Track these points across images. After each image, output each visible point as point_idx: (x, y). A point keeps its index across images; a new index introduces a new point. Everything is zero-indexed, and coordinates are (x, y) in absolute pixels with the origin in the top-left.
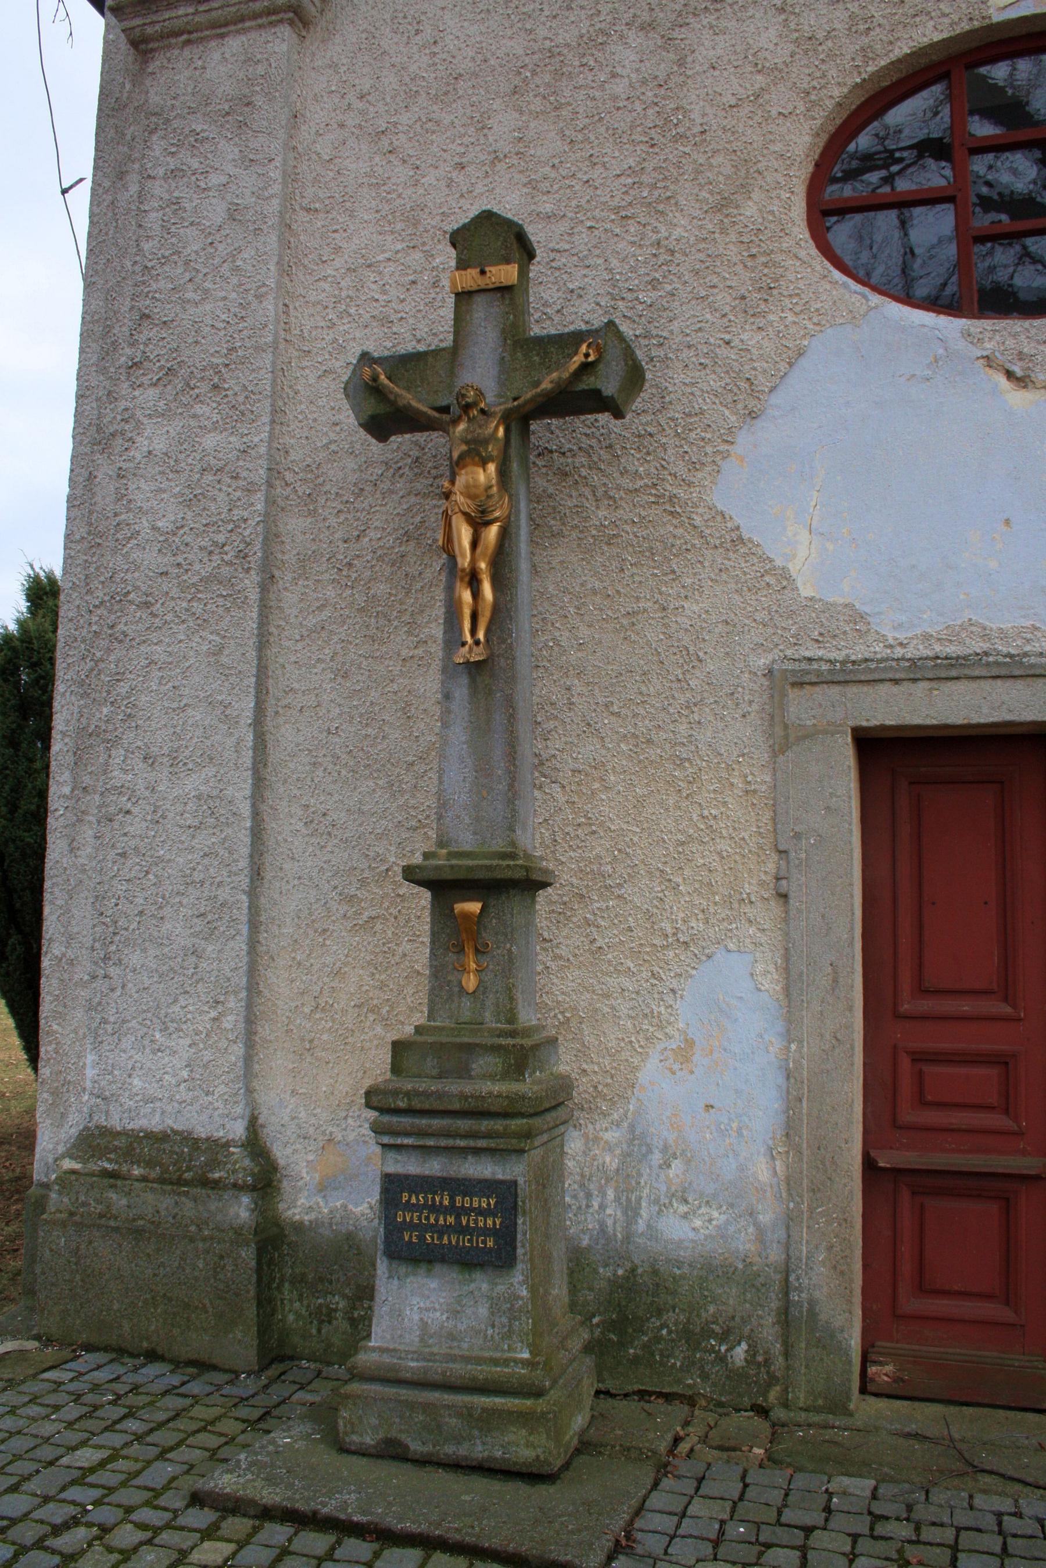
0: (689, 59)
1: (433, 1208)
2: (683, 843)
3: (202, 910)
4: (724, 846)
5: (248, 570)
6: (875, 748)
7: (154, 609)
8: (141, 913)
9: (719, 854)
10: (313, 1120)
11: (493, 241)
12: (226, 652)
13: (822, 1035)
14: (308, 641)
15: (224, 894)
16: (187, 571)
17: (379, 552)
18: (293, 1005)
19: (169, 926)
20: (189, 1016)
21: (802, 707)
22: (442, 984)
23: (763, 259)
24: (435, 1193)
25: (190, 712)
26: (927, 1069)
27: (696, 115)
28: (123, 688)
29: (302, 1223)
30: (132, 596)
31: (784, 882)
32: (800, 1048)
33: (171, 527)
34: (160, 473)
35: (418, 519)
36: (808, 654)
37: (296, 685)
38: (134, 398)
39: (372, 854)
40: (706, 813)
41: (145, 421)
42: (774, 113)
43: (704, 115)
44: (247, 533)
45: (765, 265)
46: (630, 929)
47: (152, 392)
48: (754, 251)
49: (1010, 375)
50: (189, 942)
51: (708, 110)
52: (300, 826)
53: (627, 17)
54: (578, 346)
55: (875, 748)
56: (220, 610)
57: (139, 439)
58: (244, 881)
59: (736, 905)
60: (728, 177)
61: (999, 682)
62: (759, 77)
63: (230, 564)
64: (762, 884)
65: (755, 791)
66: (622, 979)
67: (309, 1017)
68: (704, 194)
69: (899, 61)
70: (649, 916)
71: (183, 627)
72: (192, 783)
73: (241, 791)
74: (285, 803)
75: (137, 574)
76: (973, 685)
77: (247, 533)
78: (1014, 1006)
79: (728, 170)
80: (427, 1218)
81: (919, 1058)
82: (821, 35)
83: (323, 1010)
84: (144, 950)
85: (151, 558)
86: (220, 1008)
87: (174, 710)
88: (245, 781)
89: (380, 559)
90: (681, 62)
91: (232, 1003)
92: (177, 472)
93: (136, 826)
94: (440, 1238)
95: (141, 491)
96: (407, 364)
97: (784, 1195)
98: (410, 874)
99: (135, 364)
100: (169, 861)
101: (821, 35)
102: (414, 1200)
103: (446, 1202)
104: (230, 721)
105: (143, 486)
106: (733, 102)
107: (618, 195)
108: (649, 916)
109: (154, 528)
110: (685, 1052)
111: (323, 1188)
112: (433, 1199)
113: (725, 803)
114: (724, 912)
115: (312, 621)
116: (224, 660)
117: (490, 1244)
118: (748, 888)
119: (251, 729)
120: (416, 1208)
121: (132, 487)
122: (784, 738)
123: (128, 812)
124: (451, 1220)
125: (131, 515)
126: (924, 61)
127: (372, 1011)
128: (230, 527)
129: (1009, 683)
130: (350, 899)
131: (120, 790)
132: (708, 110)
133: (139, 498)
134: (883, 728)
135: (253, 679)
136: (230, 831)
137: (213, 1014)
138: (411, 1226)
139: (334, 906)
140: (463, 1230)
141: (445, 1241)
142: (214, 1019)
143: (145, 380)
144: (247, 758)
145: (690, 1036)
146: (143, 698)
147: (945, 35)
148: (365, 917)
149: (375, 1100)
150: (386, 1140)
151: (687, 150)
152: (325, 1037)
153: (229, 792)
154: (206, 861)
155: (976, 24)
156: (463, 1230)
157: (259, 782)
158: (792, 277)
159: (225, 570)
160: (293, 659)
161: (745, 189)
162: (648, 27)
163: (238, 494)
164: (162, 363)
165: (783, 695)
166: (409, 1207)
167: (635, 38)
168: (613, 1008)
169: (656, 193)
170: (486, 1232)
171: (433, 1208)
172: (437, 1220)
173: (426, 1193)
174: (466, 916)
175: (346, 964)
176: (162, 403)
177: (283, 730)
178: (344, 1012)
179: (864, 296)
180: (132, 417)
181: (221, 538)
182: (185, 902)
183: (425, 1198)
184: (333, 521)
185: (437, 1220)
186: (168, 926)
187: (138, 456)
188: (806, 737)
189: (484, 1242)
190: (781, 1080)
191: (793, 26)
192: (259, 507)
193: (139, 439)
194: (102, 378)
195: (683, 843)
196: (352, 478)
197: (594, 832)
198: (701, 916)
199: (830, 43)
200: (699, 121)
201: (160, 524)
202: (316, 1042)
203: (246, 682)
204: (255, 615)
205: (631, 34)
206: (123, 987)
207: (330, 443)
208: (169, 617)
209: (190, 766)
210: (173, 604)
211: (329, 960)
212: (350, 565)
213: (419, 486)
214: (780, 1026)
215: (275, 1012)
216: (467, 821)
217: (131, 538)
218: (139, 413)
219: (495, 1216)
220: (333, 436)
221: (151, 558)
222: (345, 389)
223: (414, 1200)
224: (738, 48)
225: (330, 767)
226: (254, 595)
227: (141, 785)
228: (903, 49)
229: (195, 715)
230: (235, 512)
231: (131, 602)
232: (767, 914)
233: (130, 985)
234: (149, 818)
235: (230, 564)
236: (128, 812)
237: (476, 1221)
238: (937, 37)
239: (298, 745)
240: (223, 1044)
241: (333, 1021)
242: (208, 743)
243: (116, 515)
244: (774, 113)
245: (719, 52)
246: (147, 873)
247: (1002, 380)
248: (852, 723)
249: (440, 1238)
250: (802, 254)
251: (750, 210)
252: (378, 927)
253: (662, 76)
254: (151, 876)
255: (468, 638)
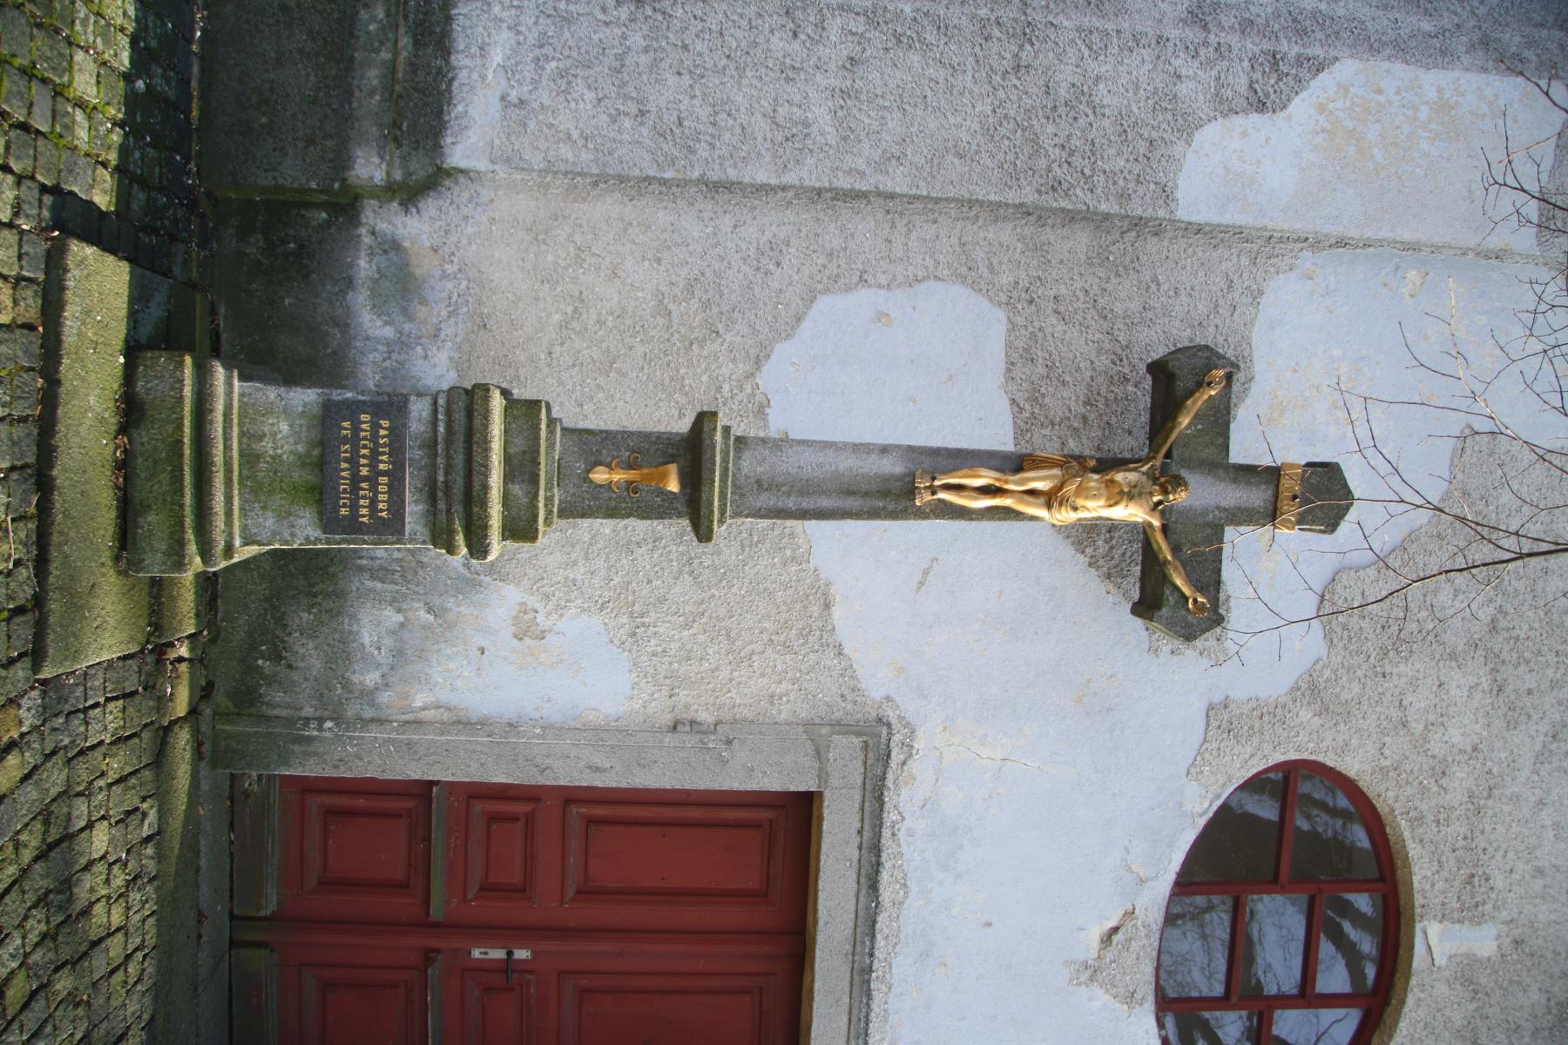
0: (1453, 664)
1: (375, 454)
2: (728, 635)
3: (686, 123)
4: (724, 673)
5: (1039, 192)
6: (801, 811)
7: (1012, 77)
8: (685, 47)
9: (717, 669)
10: (464, 241)
11: (1322, 494)
12: (956, 161)
13: (548, 756)
14: (959, 250)
15: (703, 151)
16: (1048, 118)
17: (1040, 335)
18: (584, 222)
19: (670, 82)
20: (573, 105)
21: (845, 756)
22: (595, 445)
23: (1257, 725)
24: (390, 456)
25: (898, 115)
26: (521, 824)
27: (1402, 667)
28: (930, 36)
29: (358, 224)
30: (1028, 47)
31: (688, 728)
32: (537, 736)
33: (1097, 100)
34: (1156, 89)
35: (1068, 379)
36: (894, 754)
37: (914, 235)
38: (1241, 60)
39: (736, 315)
40: (755, 658)
41: (1214, 73)
42: (1387, 740)
43: (1399, 676)
44: (1078, 191)
45: (1251, 728)
46: (650, 582)
47: (1244, 81)
48: (1266, 718)
49: (1116, 930)
50: (652, 107)
51: (1404, 680)
52: (769, 235)
53: (1508, 608)
54: (1200, 589)
55: (801, 811)
56: (1001, 156)
57: (1196, 63)
58: (715, 175)
59: (668, 681)
60: (1338, 696)
61: (852, 916)
62: (1421, 727)
63: (1049, 170)
64: (687, 706)
65: (772, 703)
66: (603, 573)
67: (570, 239)
68: (1327, 673)
69: (1404, 846)
70: (662, 600)
71: (988, 109)
72: (820, 113)
73: (809, 173)
74: (792, 218)
75: (1051, 55)
76: (852, 895)
77: (1078, 191)
78: (573, 900)
79: (1344, 696)
80: (365, 447)
81: (530, 818)
82: (1444, 782)
83: (578, 256)
84: (646, 50)
85: (1066, 75)
86: (581, 143)
87: (901, 96)
88: (818, 179)
89: (1033, 336)
90: (1453, 656)
91: (586, 156)
92: (1154, 110)
93: (779, 43)
94: (346, 460)
95: (1140, 65)
96: (1219, 420)
97: (404, 717)
98: (704, 420)
99: (1276, 64)
100: (739, 84)
101: (1444, 782)
102: (382, 432)
103: (381, 466)
104: (880, 166)
105: (1144, 69)
106: (1405, 703)
107: (1346, 593)
108: (662, 600)
109: (1098, 79)
110: (882, 317)
111: (393, 247)
112: (384, 453)
113: (762, 675)
114: (662, 669)
115: (979, 255)
116: (950, 158)
117: (344, 511)
118: (683, 696)
119: (872, 188)
120: (374, 437)
121: (1146, 53)
122: (817, 734)
123: (795, 35)
124: (364, 471)
125: (1115, 51)
126: (1399, 863)
127: (576, 310)
128: (1087, 172)
129: (851, 924)
130: (690, 288)
131: (821, 26)
132: (1404, 680)
133: (1131, 61)
134: (821, 819)
135: (925, 193)
136: (767, 159)
137: (575, 134)
138: (356, 429)
139: (684, 273)
140: (355, 488)
141: (344, 465)
142: (569, 136)
143: (1257, 75)
144: (843, 183)
145: (549, 636)
146: (916, 58)
147: (1416, 885)
148: (672, 307)
149: (479, 393)
150: (441, 402)
151: (1372, 660)
152: (550, 258)
153: (810, 161)
154: (738, 130)
155: (1418, 911)
156: (355, 488)
157: (816, 194)
158: (1235, 751)
159: (1042, 163)
160: (942, 234)
161: (1324, 711)
162: (1493, 627)
163: (1121, 183)
164: (1273, 96)
165: (858, 734)
166: (375, 427)
167: (1485, 614)
168: (575, 562)
169: (1339, 630)
170: (354, 507)
171: (375, 454)
172: (364, 456)
173: (390, 445)
174: (664, 477)
175: (623, 283)
176: (1230, 93)
177: (870, 218)
178: (575, 280)
179: (1206, 812)
180: (1222, 57)
181: (1077, 161)
182: (695, 102)
183: (384, 445)
184: (1078, 284)
185: (364, 456)
186: (672, 80)
187: (1177, 63)
188: (818, 753)
189: (344, 505)
190: (507, 717)
191: (1458, 758)
192: (1104, 207)
193: (1196, 63)
194: (1270, 10)
195: (728, 635)
196: (1119, 308)
197: (743, 549)
198: (659, 649)
199: (1435, 789)
200: (1395, 671)
201: (1101, 86)
202: (544, 247)
203: (922, 184)
204: (992, 197)
205: (1491, 610)
206: (607, 24)
207: (1158, 284)
208: (1001, 94)
209: (840, 113)
210: (1014, 98)
211: (629, 263)
212: (1031, 302)
213: (1100, 380)
214: (556, 718)
215: (575, 200)
216: (759, 469)
217: (1090, 49)
218: (1225, 64)
219: (371, 516)
220: (1164, 287)
221: (1066, 75)
222: (1207, 347)
223: (382, 432)
224: (1452, 709)
225: (827, 272)
226: (1012, 197)
227: (822, 51)
228: (1413, 850)
229: (894, 123)
230: (1102, 178)
231: (1021, 47)
232: (660, 708)
233: (608, 31)
234: (788, 61)
235: (1049, 170)
236: (795, 35)
237: (364, 497)
238: (1416, 880)
239: (852, 235)
240: (543, 145)
241: (566, 268)
242: (863, 135)
243: (1118, 32)
244: (1387, 740)
245: (1452, 692)
246: (728, 57)
247: (1113, 923)
248: (827, 794)
249: (346, 460)
250: (1254, 761)
251: (1305, 715)
252: (661, 321)
253: (1443, 637)
254: (724, 61)
255: (937, 483)
